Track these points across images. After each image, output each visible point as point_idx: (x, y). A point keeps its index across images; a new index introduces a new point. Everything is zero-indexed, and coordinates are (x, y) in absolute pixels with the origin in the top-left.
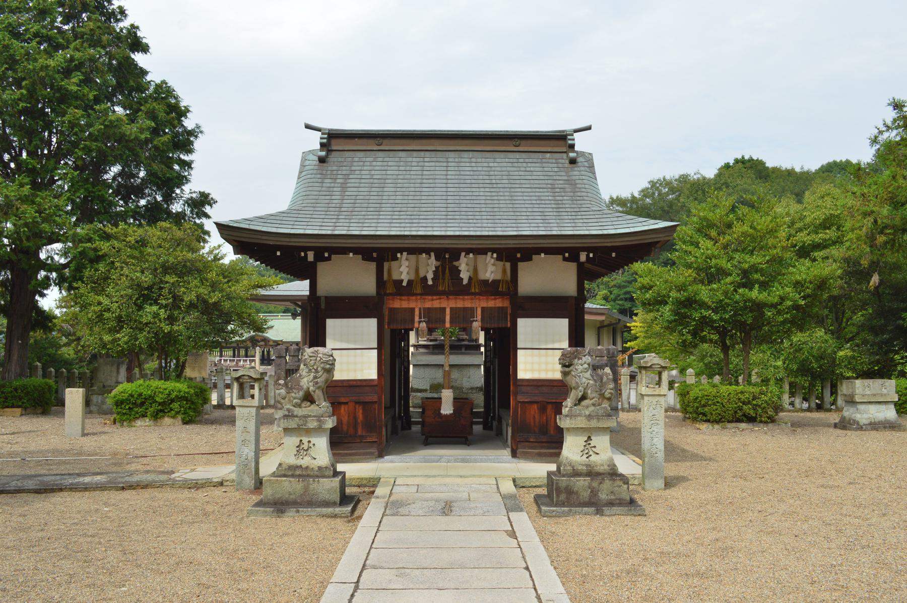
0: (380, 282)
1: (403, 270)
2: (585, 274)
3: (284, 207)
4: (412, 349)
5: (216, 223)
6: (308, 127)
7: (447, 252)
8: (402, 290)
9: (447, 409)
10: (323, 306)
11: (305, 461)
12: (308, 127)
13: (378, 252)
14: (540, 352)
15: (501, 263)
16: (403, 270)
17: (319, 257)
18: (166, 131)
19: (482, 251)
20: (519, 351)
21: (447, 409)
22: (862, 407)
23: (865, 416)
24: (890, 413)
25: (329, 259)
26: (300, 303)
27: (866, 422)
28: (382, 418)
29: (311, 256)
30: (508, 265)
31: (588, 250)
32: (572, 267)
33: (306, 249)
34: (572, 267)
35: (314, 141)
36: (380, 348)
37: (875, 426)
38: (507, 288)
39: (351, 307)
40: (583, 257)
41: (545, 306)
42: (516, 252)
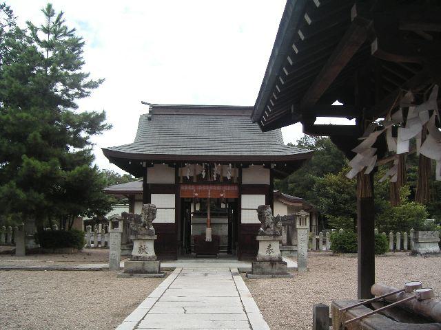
0: (177, 178)
1: (188, 172)
2: (273, 175)
3: (133, 142)
4: (192, 215)
5: (103, 149)
6: (143, 103)
7: (209, 162)
8: (188, 181)
9: (208, 238)
10: (149, 188)
11: (143, 254)
12: (143, 103)
13: (176, 163)
14: (250, 208)
15: (234, 169)
16: (188, 172)
17: (149, 165)
18: (373, 282)
19: (227, 163)
20: (242, 211)
21: (208, 238)
22: (422, 245)
23: (424, 249)
24: (436, 248)
25: (152, 166)
26: (128, 195)
27: (424, 252)
28: (177, 244)
29: (144, 165)
30: (237, 170)
31: (275, 162)
32: (268, 170)
33: (143, 161)
34: (268, 170)
35: (146, 110)
36: (176, 208)
37: (427, 255)
38: (238, 182)
39: (162, 189)
40: (272, 167)
41: (254, 190)
42: (241, 163)
